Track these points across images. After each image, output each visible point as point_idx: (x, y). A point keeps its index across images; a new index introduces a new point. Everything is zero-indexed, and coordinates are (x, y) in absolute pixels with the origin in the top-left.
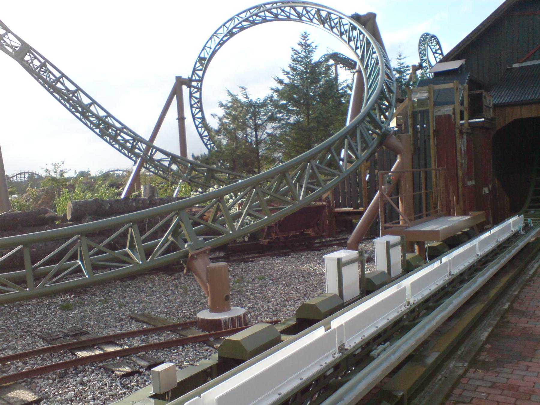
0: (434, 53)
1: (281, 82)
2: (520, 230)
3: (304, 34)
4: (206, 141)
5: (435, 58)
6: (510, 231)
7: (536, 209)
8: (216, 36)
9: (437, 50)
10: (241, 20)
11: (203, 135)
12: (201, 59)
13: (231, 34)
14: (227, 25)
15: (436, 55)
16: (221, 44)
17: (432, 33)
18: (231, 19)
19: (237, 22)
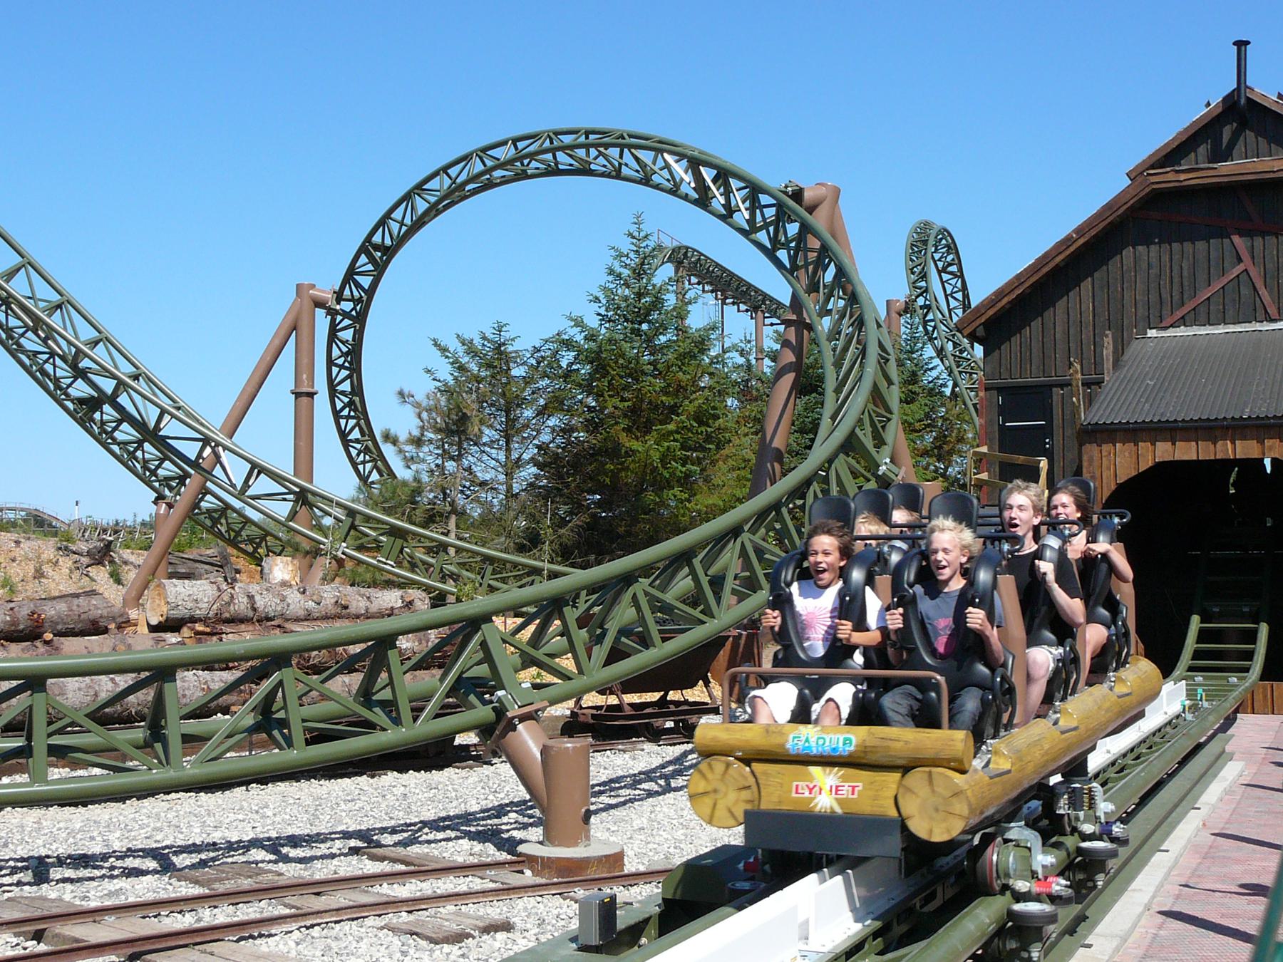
0: (939, 272)
1: (578, 323)
2: (1184, 712)
3: (633, 229)
4: (339, 405)
5: (943, 283)
6: (1162, 712)
7: (932, 635)
8: (419, 195)
9: (950, 265)
10: (489, 163)
11: (340, 388)
12: (366, 248)
13: (456, 195)
14: (453, 172)
15: (945, 277)
16: (434, 211)
17: (939, 221)
18: (466, 158)
19: (479, 167)
